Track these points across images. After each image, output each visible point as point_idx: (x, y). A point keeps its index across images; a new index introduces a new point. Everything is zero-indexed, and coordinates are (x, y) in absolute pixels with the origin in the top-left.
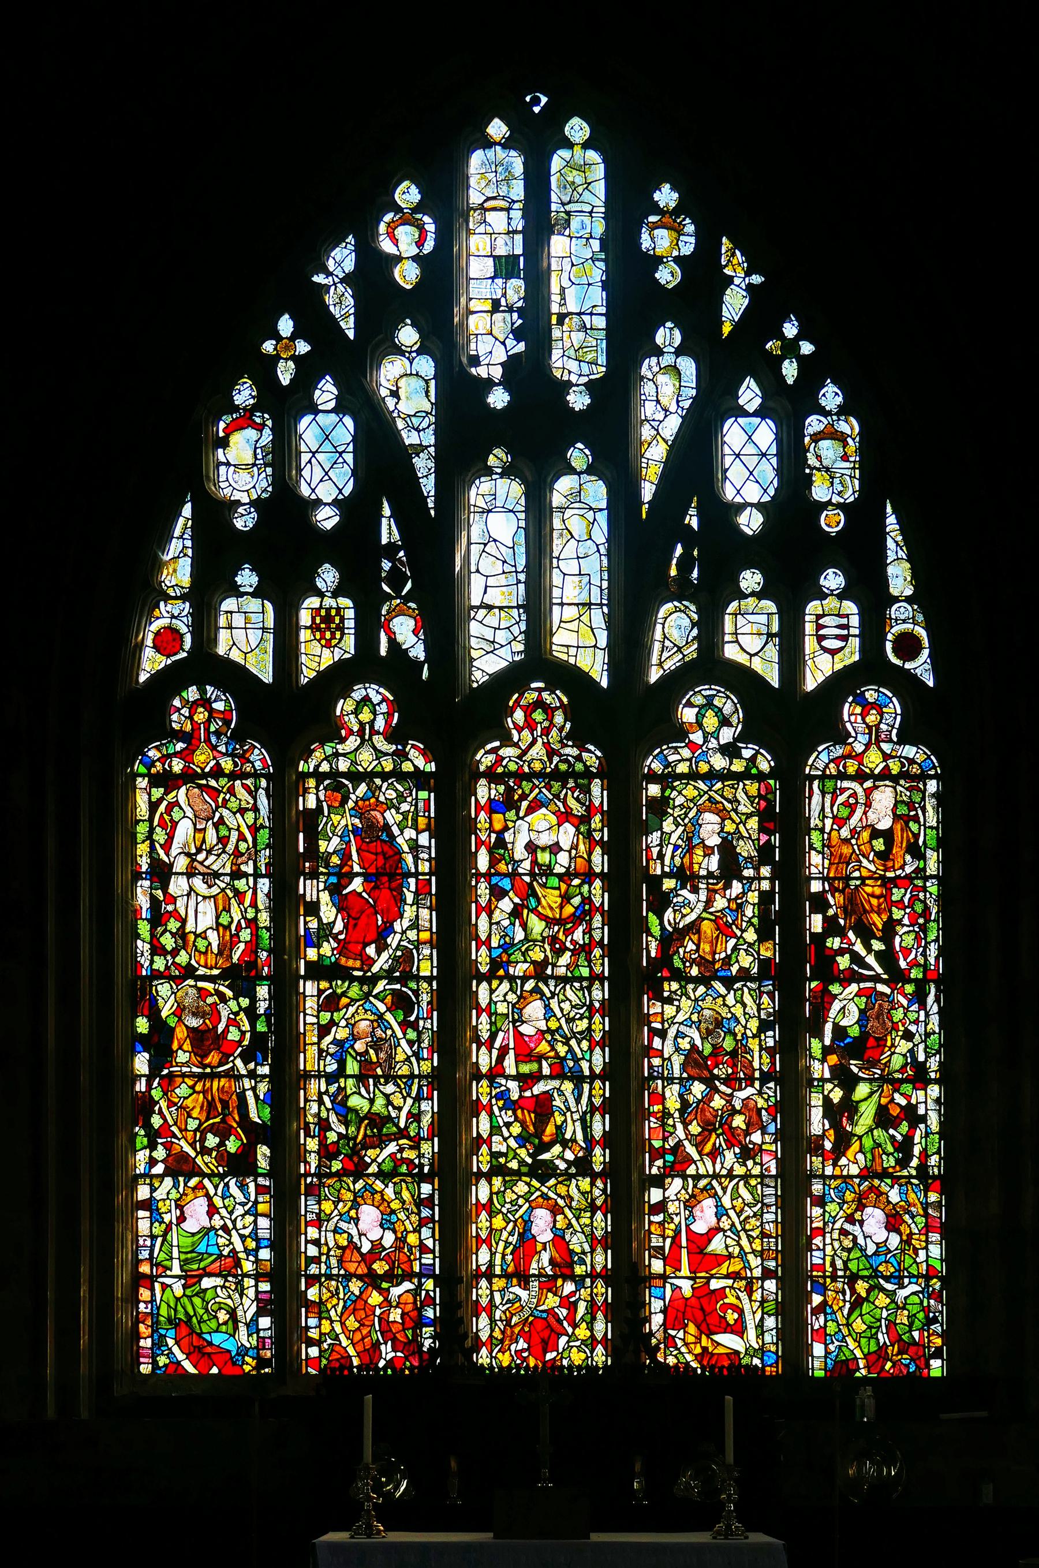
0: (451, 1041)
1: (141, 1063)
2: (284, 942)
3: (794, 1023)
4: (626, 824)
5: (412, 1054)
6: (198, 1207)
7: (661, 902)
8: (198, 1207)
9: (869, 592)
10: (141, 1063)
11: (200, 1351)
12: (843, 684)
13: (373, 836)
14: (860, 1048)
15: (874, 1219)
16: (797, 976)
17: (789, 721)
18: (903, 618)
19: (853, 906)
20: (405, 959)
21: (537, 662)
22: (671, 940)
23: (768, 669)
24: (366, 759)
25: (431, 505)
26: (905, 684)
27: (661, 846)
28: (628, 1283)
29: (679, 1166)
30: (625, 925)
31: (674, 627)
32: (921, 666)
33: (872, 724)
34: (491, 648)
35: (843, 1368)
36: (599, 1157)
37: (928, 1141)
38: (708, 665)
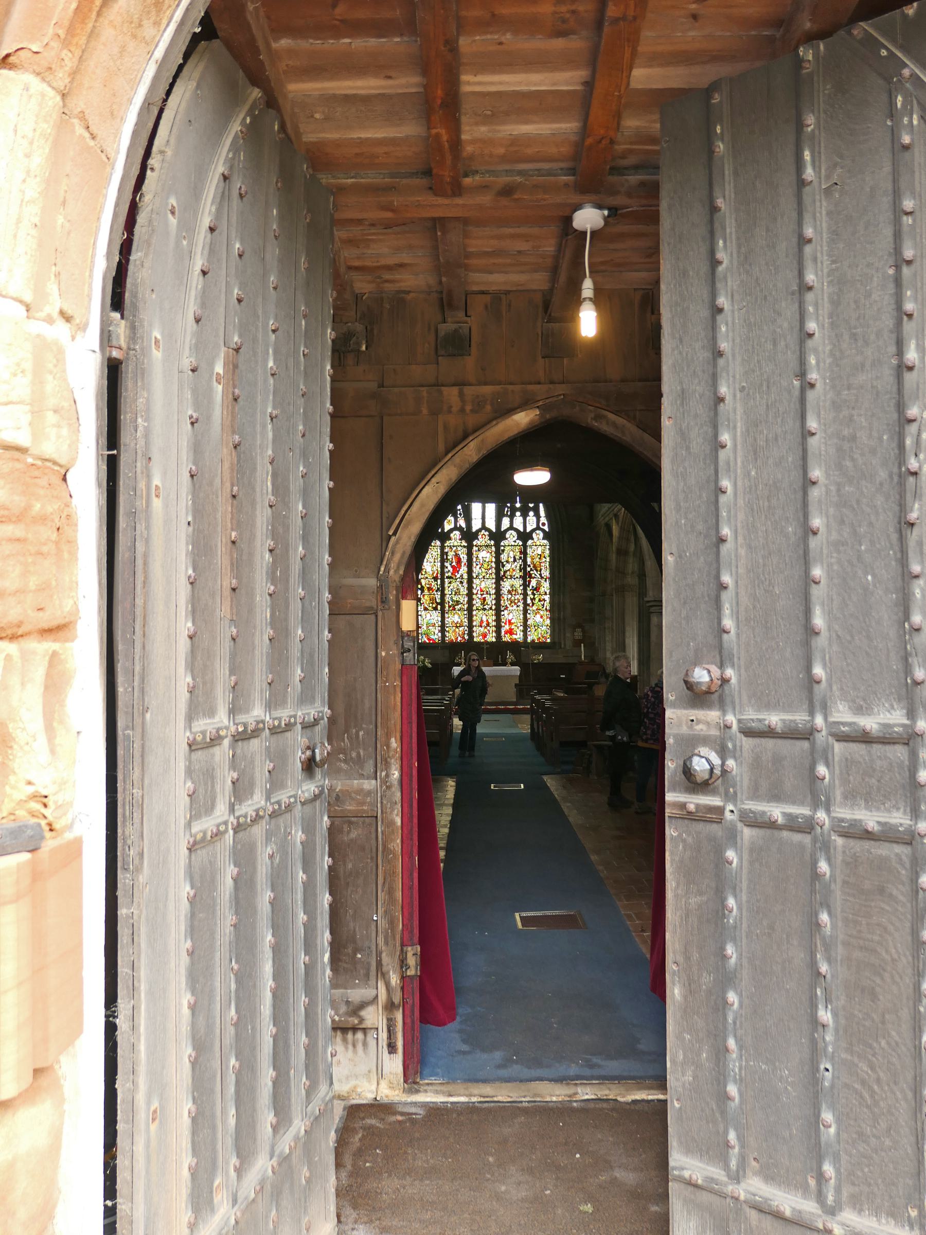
0: (470, 588)
1: (419, 592)
2: (443, 573)
3: (525, 585)
4: (498, 553)
5: (463, 590)
6: (428, 615)
7: (503, 566)
8: (428, 615)
9: (537, 516)
10: (419, 592)
11: (429, 639)
12: (533, 530)
13: (457, 555)
14: (537, 589)
15: (538, 616)
16: (526, 577)
17: (525, 536)
18: (543, 520)
19: (535, 566)
20: (462, 576)
21: (484, 527)
22: (505, 572)
23: (521, 530)
24: (456, 544)
25: (442, 844)
26: (543, 531)
27: (504, 557)
28: (498, 627)
29: (506, 608)
30: (498, 570)
31: (506, 523)
32: (546, 528)
33: (538, 536)
34: (476, 525)
35: (533, 641)
36: (494, 607)
37: (547, 605)
38: (511, 528)
